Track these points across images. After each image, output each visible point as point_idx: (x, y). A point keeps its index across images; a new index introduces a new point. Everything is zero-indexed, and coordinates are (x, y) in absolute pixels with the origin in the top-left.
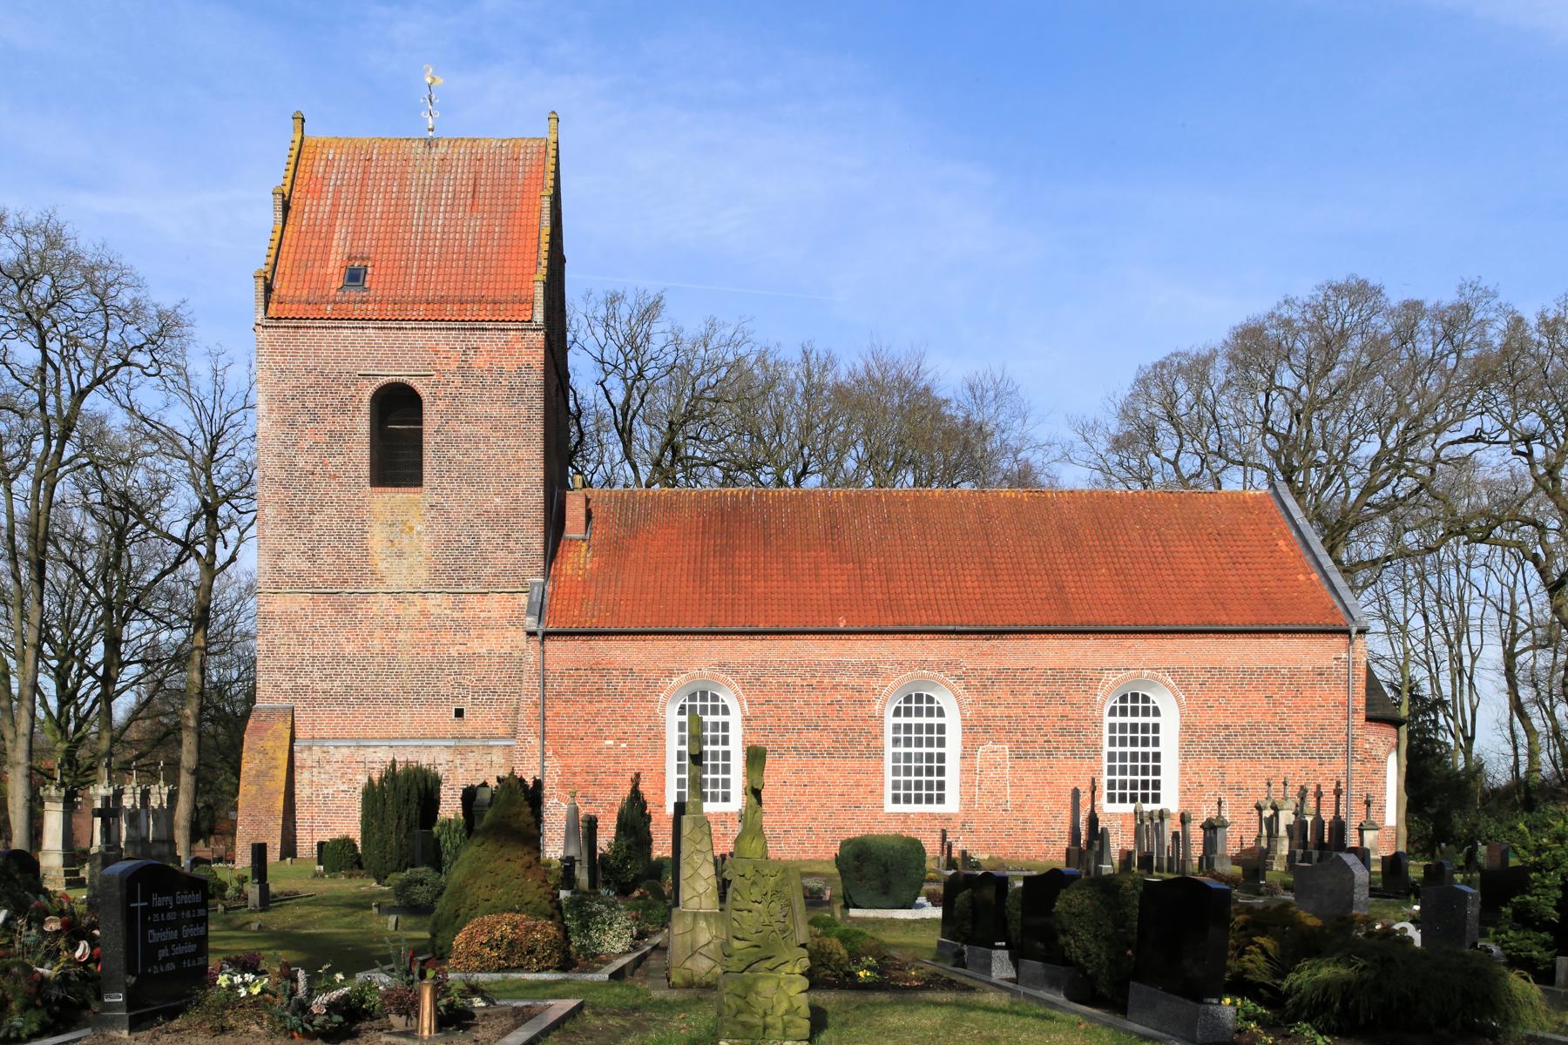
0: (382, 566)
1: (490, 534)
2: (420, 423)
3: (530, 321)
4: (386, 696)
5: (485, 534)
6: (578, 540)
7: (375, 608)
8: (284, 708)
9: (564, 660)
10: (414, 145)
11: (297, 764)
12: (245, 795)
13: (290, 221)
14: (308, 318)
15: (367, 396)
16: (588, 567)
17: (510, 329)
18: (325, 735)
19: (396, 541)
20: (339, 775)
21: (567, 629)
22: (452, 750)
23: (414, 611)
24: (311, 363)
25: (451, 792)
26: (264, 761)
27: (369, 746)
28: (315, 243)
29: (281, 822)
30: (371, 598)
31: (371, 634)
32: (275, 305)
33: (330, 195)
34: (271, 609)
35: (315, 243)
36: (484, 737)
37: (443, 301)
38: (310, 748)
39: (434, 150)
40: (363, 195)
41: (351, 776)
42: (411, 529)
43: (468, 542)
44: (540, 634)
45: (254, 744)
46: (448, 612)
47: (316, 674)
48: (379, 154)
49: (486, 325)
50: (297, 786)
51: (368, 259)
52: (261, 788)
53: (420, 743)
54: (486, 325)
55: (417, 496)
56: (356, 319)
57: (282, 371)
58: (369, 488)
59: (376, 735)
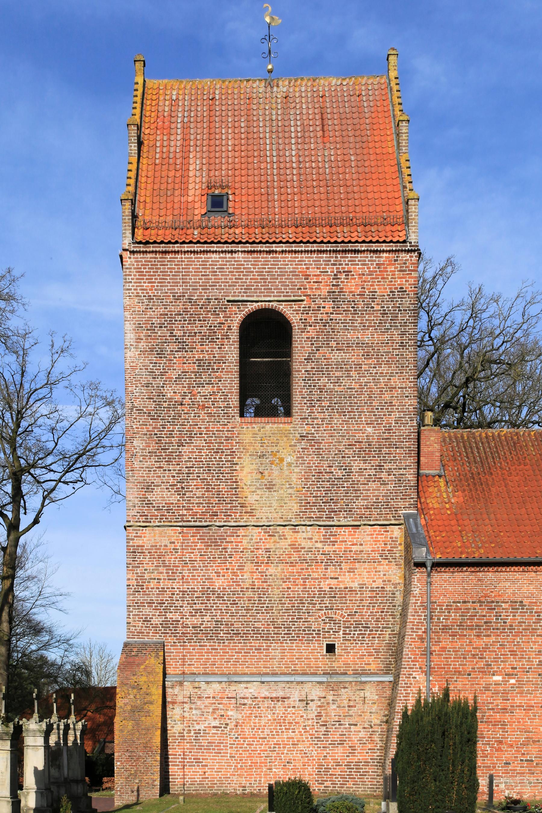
0: (252, 499)
1: (362, 465)
2: (289, 354)
3: (405, 242)
4: (256, 630)
5: (356, 465)
6: (434, 476)
7: (245, 542)
8: (155, 644)
9: (451, 592)
10: (255, 85)
11: (169, 699)
12: (122, 731)
13: (144, 155)
14: (176, 242)
15: (235, 326)
16: (453, 501)
17: (383, 251)
18: (195, 670)
19: (266, 473)
20: (211, 710)
21: (457, 559)
22: (324, 687)
23: (284, 544)
24: (179, 290)
25: (324, 728)
26: (138, 697)
27: (240, 682)
28: (171, 174)
29: (158, 758)
30: (241, 532)
31: (241, 568)
32: (141, 231)
33: (179, 131)
34: (141, 543)
35: (171, 174)
36: (356, 673)
37: (310, 223)
38: (181, 683)
39: (275, 89)
40: (212, 131)
41: (222, 712)
42: (282, 460)
43: (340, 474)
44: (429, 564)
45: (127, 679)
46: (319, 545)
47: (186, 609)
48: (221, 94)
49: (359, 247)
50: (169, 721)
51: (228, 187)
52: (137, 723)
53: (292, 679)
54: (359, 247)
55: (287, 426)
56: (226, 243)
57: (150, 299)
58: (238, 419)
59: (246, 670)
